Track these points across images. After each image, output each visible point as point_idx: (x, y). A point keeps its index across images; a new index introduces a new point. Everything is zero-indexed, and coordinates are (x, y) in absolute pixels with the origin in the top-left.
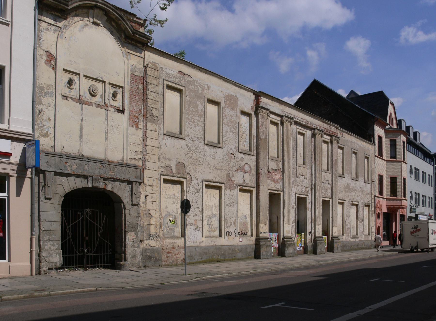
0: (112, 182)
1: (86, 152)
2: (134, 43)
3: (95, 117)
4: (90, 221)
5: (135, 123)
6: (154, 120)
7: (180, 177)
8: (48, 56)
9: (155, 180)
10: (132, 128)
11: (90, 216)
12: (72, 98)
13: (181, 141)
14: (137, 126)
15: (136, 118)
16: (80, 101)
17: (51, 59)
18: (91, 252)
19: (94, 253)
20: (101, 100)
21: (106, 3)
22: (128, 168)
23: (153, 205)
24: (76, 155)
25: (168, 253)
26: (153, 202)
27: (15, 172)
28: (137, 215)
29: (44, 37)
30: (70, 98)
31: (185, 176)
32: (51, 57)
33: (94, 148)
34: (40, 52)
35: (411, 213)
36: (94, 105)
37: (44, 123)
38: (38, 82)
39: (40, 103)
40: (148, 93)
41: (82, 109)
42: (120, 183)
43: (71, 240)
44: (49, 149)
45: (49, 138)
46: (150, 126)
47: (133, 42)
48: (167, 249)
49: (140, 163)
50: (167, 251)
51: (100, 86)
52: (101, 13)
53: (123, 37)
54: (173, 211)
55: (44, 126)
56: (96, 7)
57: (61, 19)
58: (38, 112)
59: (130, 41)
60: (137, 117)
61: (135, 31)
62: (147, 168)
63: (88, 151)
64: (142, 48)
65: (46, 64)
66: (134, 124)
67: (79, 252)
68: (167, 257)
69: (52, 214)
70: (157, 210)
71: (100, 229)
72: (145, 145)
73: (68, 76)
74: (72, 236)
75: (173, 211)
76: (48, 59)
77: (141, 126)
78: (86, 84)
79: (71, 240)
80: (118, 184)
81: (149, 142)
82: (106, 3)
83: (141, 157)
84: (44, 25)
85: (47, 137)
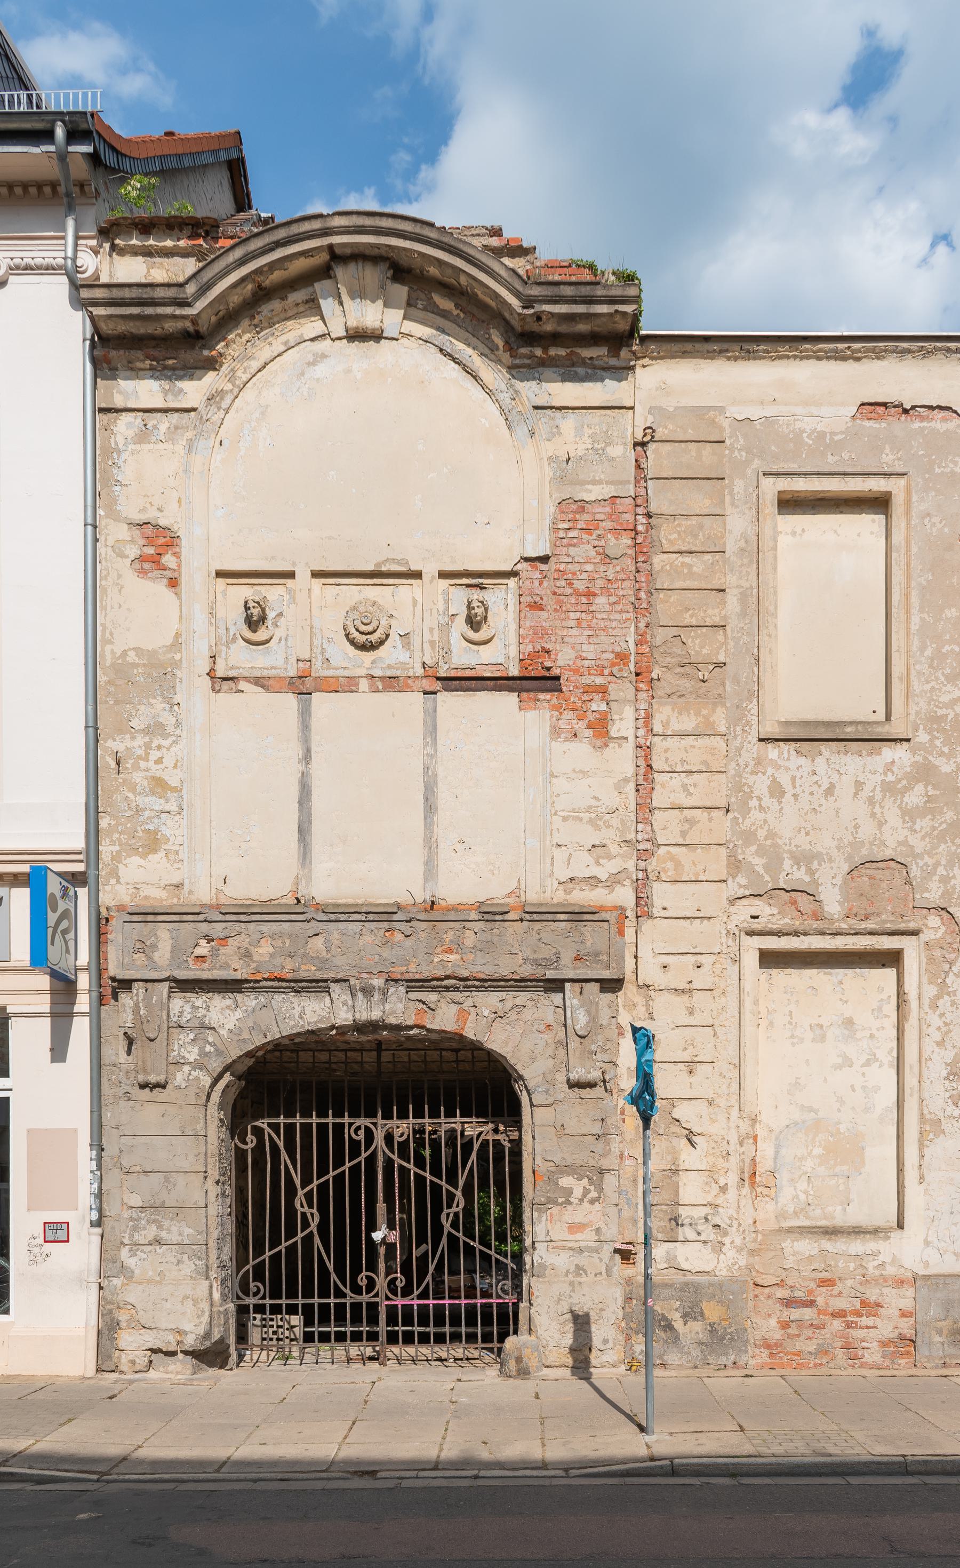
0: (457, 996)
1: (325, 887)
2: (562, 352)
3: (369, 734)
4: (401, 1168)
5: (591, 717)
6: (704, 675)
7: (872, 933)
8: (150, 541)
9: (706, 960)
10: (573, 746)
11: (404, 1146)
12: (259, 681)
13: (889, 752)
14: (600, 728)
15: (597, 697)
16: (302, 685)
17: (158, 548)
18: (407, 1292)
19: (420, 1297)
20: (404, 656)
21: (368, 221)
22: (537, 926)
23: (693, 1079)
24: (284, 901)
25: (789, 1303)
26: (691, 1065)
27: (47, 998)
28: (597, 1129)
29: (126, 473)
30: (246, 679)
31: (912, 925)
32: (162, 541)
33: (366, 864)
34: (115, 532)
35: (571, 1189)
36: (364, 684)
37: (142, 801)
38: (107, 654)
39: (124, 728)
40: (657, 567)
41: (305, 714)
42: (503, 995)
43: (317, 1240)
44: (163, 894)
45: (162, 854)
46: (666, 716)
47: (553, 352)
48: (781, 1284)
49: (625, 896)
50: (781, 1293)
51: (396, 599)
52: (371, 275)
53: (500, 342)
54: (841, 1101)
55: (139, 810)
56: (336, 257)
57: (198, 372)
58: (113, 764)
59: (538, 352)
60: (603, 691)
61: (535, 291)
62: (657, 911)
63: (334, 879)
64: (613, 362)
65: (142, 572)
66: (582, 724)
67: (357, 1290)
68: (785, 1325)
69: (188, 1151)
70: (722, 1102)
71: (451, 1197)
72: (645, 809)
73: (242, 592)
74: (323, 1229)
75: (841, 1101)
76: (151, 551)
77: (624, 723)
78: (334, 605)
79: (317, 1240)
80: (489, 1001)
81: (667, 790)
82: (368, 221)
83: (631, 864)
84: (125, 426)
85: (154, 851)
